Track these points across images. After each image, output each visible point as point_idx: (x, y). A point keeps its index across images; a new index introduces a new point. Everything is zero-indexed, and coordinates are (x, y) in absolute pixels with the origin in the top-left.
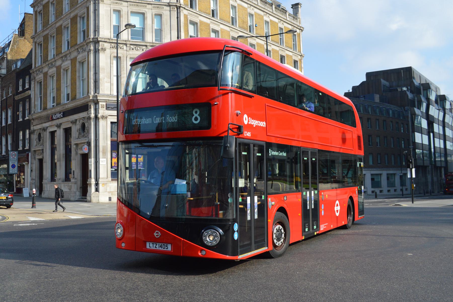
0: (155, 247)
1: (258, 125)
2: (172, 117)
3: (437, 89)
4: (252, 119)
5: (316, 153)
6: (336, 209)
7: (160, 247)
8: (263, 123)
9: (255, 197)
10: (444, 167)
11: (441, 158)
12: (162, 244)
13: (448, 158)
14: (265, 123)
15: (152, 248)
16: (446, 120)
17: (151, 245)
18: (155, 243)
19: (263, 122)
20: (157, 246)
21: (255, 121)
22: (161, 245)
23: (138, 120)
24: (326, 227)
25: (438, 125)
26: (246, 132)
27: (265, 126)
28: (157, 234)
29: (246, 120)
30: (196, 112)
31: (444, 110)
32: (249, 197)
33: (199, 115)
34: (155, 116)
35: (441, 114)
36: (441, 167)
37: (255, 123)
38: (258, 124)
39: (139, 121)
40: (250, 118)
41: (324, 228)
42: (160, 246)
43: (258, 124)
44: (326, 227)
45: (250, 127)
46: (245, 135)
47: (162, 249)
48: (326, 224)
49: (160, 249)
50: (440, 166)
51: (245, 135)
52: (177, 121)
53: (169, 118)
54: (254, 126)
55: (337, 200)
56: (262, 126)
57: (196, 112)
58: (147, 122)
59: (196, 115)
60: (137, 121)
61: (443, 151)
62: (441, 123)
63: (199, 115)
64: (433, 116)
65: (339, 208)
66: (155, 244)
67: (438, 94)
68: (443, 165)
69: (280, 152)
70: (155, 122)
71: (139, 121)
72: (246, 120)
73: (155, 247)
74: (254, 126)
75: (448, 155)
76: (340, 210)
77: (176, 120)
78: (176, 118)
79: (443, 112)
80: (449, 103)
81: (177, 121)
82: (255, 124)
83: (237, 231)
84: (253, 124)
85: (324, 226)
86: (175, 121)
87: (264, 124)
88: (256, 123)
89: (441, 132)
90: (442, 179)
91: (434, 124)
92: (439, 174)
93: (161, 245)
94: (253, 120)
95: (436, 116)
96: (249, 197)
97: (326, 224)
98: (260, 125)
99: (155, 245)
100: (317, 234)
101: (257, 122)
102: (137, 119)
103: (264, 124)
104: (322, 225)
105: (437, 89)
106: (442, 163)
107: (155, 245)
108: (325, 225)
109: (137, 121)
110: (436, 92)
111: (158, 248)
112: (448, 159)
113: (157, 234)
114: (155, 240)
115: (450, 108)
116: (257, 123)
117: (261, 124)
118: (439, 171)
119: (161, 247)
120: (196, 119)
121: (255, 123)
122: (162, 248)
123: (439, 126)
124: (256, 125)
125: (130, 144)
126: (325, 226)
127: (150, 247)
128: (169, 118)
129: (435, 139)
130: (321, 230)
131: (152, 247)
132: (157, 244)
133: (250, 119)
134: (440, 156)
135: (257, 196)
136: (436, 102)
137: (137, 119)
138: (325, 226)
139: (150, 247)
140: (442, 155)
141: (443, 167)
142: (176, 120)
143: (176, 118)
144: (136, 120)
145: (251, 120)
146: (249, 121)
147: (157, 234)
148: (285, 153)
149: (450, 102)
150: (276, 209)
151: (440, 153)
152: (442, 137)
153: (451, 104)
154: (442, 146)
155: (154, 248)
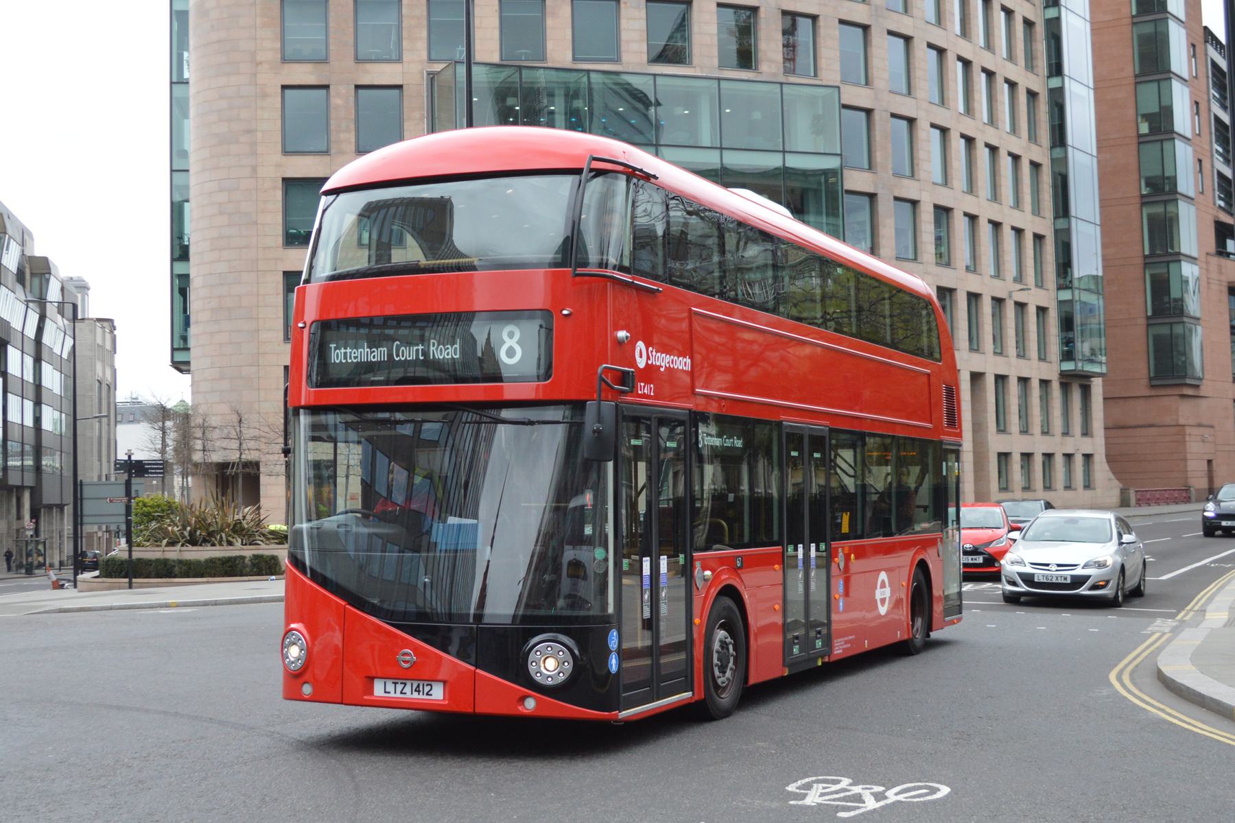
0: (401, 693)
1: (672, 366)
2: (444, 346)
3: (24, 237)
4: (657, 352)
5: (824, 437)
6: (887, 591)
7: (416, 691)
8: (685, 360)
9: (662, 557)
10: (31, 488)
11: (22, 460)
12: (421, 683)
13: (44, 458)
14: (689, 361)
15: (392, 695)
16: (47, 339)
17: (390, 687)
18: (399, 681)
19: (685, 357)
20: (408, 689)
21: (664, 355)
22: (418, 686)
23: (349, 350)
24: (849, 645)
25: (19, 353)
26: (643, 384)
27: (688, 368)
28: (407, 657)
29: (641, 356)
30: (511, 335)
31: (42, 302)
32: (648, 558)
33: (517, 342)
34: (398, 343)
35: (33, 318)
36: (20, 489)
37: (663, 360)
38: (672, 363)
39: (353, 355)
40: (650, 349)
41: (843, 650)
42: (414, 689)
43: (672, 363)
44: (849, 645)
45: (650, 373)
46: (640, 392)
47: (421, 696)
48: (851, 637)
49: (415, 695)
50: (20, 484)
51: (640, 392)
52: (458, 356)
53: (437, 349)
54: (662, 370)
55: (880, 570)
56: (680, 368)
57: (511, 335)
58: (374, 357)
59: (509, 342)
60: (345, 354)
61: (30, 437)
62: (30, 347)
63: (517, 342)
64: (9, 323)
65: (879, 594)
66: (401, 683)
67: (28, 253)
68: (29, 480)
69: (728, 438)
70: (397, 359)
71: (351, 353)
72: (641, 356)
73: (401, 693)
74: (662, 370)
75: (43, 449)
76: (890, 597)
77: (403, 351)
78: (456, 349)
79: (38, 310)
80: (836, 565)
81: (458, 356)
82: (663, 364)
83: (611, 651)
84: (658, 364)
85: (843, 643)
86: (455, 357)
87: (685, 363)
88: (667, 361)
89: (29, 377)
90: (24, 528)
91: (10, 349)
92: (14, 511)
93: (418, 686)
94: (659, 354)
95: (16, 324)
96: (648, 558)
97: (851, 637)
98: (676, 367)
99: (399, 687)
100: (822, 663)
101: (668, 358)
102: (345, 349)
103: (685, 363)
104: (839, 640)
105: (26, 237)
106: (25, 473)
107: (399, 687)
108: (846, 639)
109: (345, 354)
110: (23, 244)
111: (409, 695)
112: (44, 463)
113: (407, 658)
114: (400, 677)
115: (61, 301)
116: (669, 363)
117: (678, 363)
118: (14, 500)
119: (419, 691)
120: (511, 352)
121: (663, 360)
122: (421, 693)
123: (25, 356)
124: (667, 365)
125: (326, 414)
126: (846, 642)
127: (385, 692)
128: (437, 349)
129: (10, 396)
130: (835, 652)
131: (393, 691)
132: (405, 684)
133: (652, 352)
134: (22, 454)
135: (666, 557)
136: (20, 277)
137: (345, 349)
138: (846, 642)
139: (385, 692)
140: (27, 448)
141: (27, 487)
142: (456, 354)
143: (456, 349)
144: (343, 350)
145: (654, 353)
146: (648, 358)
147: (407, 658)
148: (738, 439)
149: (62, 283)
150: (714, 591)
151: (23, 444)
152: (30, 391)
153: (62, 289)
154: (29, 422)
155: (398, 695)
